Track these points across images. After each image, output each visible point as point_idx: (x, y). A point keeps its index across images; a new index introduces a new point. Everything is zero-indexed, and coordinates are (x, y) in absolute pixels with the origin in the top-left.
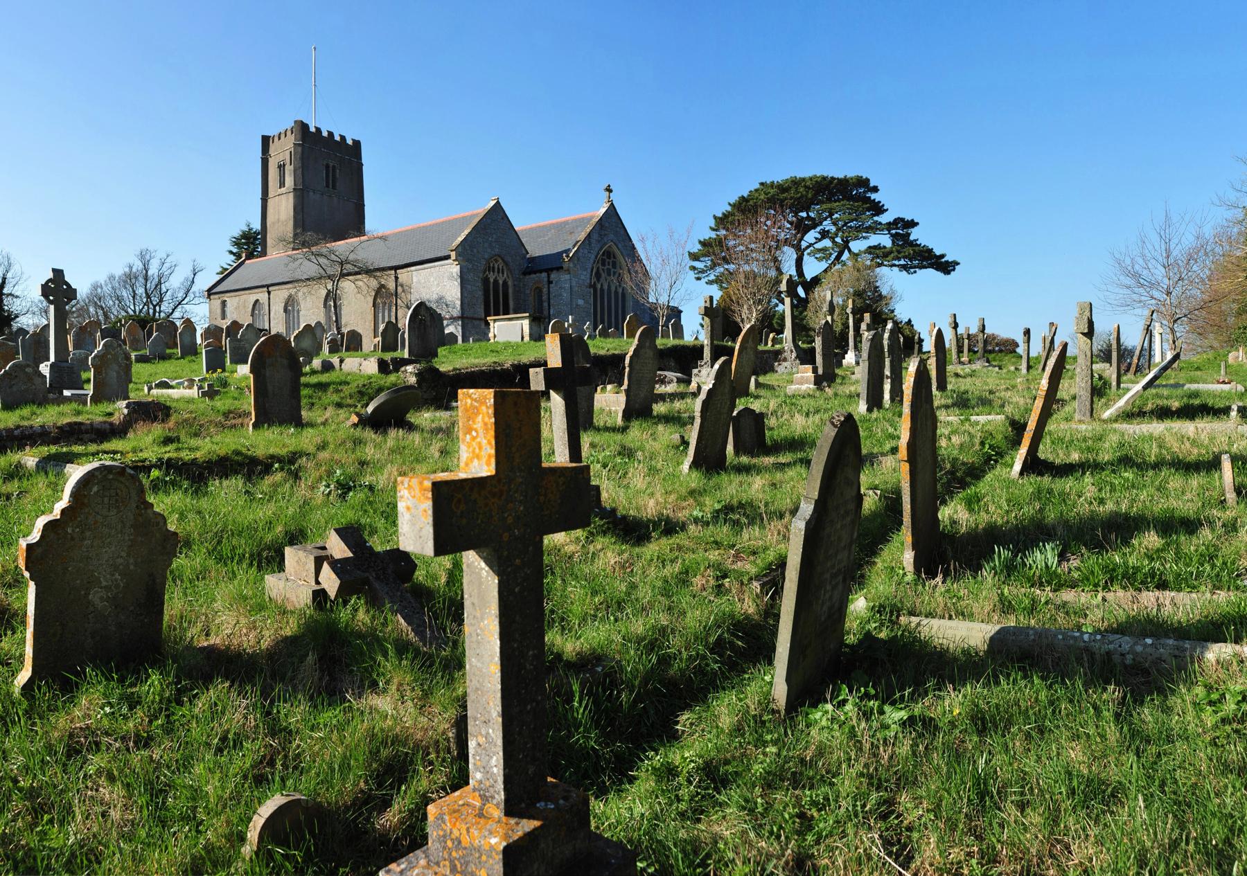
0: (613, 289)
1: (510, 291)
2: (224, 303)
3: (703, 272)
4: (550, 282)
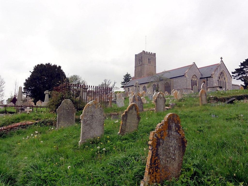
0: (223, 81)
1: (197, 83)
2: (129, 88)
3: (236, 76)
4: (207, 80)
